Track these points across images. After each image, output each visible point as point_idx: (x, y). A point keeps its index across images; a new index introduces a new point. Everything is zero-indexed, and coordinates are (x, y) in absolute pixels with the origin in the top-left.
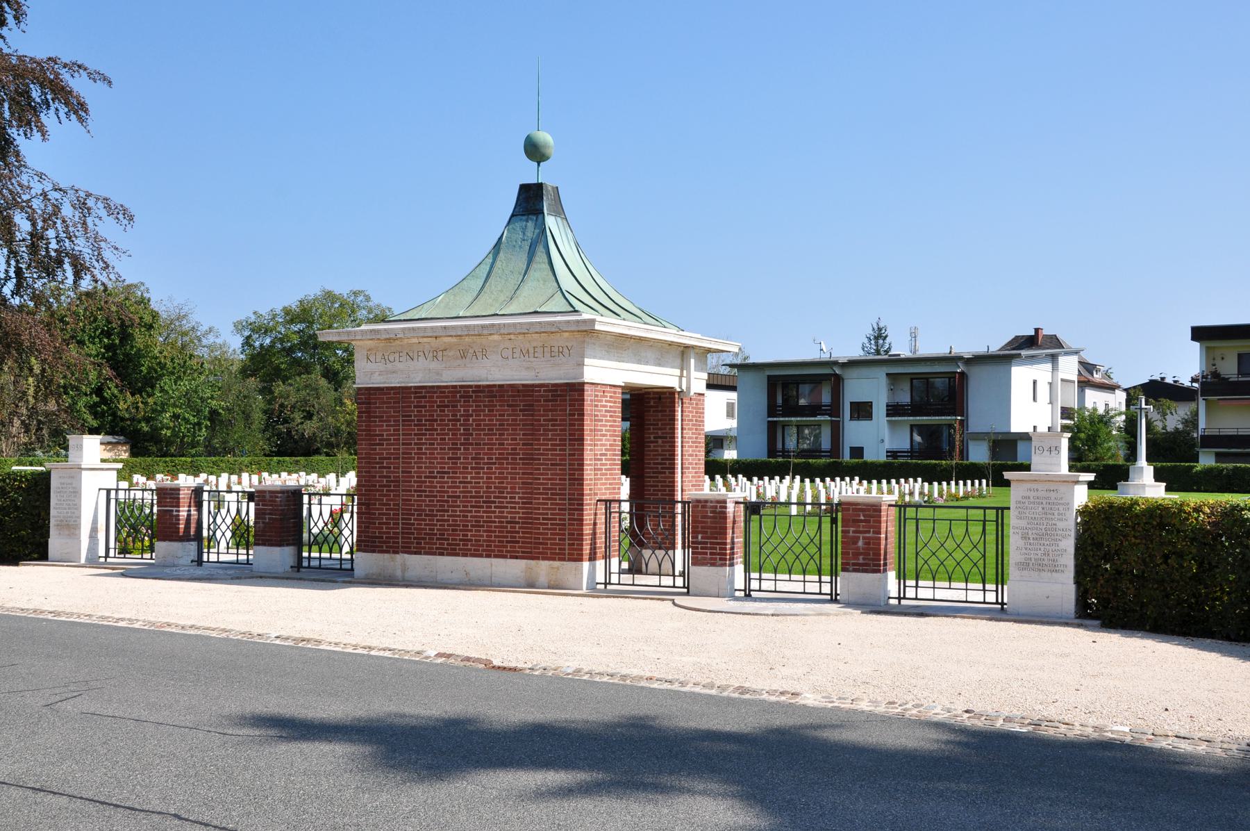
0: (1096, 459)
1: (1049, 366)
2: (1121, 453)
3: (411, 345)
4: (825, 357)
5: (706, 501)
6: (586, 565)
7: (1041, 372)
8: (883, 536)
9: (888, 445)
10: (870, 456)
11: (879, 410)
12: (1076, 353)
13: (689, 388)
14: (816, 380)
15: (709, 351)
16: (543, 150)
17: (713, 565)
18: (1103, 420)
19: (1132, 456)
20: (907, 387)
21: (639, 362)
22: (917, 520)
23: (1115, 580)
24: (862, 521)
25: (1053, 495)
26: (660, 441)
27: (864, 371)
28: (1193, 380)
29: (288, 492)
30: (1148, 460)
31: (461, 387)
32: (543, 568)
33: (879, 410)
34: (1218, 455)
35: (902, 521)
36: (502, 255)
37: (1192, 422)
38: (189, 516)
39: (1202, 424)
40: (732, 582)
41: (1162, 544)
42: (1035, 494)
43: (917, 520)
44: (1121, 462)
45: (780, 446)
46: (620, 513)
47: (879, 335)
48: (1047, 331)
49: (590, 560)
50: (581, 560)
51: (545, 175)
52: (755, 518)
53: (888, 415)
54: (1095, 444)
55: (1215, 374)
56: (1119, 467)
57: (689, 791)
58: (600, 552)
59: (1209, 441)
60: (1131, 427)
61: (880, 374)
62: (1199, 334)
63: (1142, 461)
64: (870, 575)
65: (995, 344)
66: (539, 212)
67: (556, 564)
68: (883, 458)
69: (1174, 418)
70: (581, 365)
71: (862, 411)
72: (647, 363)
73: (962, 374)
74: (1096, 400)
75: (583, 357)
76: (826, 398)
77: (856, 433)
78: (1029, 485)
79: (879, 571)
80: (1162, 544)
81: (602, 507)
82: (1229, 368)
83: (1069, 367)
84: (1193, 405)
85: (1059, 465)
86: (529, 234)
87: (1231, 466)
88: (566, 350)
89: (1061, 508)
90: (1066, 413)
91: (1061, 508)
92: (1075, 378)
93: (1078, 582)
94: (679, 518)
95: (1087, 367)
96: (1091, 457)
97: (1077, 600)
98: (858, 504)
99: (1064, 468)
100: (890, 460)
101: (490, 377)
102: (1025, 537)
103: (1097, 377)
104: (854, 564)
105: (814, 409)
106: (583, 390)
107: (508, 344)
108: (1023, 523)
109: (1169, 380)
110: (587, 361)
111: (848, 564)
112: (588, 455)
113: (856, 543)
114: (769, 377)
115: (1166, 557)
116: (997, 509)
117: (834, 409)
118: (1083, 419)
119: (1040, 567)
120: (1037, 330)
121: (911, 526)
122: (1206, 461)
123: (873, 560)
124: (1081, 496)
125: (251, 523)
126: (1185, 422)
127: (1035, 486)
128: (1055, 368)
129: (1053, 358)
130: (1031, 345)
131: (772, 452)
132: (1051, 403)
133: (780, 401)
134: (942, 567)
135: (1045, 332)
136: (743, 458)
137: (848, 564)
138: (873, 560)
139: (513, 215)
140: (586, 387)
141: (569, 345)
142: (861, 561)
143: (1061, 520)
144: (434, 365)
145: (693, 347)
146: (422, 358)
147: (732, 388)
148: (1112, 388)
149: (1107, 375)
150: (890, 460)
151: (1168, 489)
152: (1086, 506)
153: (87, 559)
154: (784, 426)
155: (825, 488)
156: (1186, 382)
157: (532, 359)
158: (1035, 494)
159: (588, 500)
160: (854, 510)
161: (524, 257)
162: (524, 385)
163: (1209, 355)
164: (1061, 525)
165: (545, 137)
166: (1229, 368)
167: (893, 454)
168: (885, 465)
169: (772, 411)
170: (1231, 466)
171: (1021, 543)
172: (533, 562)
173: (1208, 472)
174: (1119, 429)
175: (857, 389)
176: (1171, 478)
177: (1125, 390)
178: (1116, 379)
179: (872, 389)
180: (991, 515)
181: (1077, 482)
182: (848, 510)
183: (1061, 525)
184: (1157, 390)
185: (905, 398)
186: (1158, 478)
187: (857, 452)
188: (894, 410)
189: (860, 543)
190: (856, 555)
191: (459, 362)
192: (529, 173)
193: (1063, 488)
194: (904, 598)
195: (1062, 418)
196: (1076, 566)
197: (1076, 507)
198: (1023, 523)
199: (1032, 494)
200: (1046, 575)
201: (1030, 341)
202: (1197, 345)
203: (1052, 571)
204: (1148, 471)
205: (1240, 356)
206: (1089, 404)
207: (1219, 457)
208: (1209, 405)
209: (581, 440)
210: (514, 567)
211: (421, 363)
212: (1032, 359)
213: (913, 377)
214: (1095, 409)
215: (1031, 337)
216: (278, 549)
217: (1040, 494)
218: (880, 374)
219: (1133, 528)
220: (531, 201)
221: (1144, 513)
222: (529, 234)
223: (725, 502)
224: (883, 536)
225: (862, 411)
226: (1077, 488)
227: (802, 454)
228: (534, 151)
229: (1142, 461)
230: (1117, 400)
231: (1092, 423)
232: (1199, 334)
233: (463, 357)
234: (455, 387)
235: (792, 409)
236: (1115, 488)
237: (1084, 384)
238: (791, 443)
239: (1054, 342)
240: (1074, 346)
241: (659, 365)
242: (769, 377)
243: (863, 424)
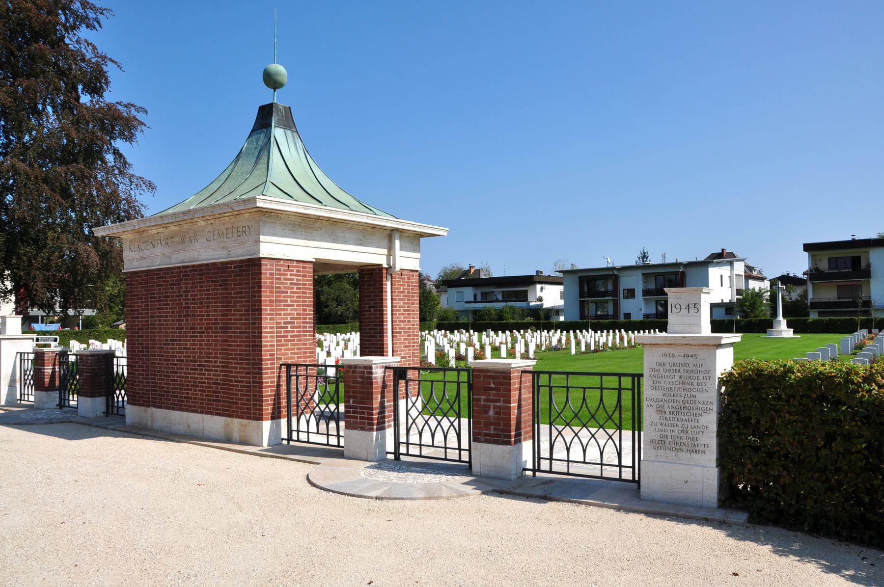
0: (755, 316)
1: (729, 267)
2: (768, 313)
3: (153, 235)
4: (610, 266)
5: (356, 367)
6: (267, 425)
7: (725, 271)
8: (514, 405)
9: (643, 312)
10: (634, 318)
11: (639, 293)
12: (743, 260)
13: (394, 264)
14: (605, 278)
15: (422, 235)
16: (275, 77)
17: (363, 429)
18: (759, 295)
19: (775, 314)
20: (653, 280)
21: (335, 241)
22: (551, 388)
23: (766, 464)
24: (492, 389)
25: (691, 361)
26: (372, 310)
27: (629, 272)
28: (804, 274)
29: (98, 355)
30: (784, 316)
31: (184, 267)
32: (236, 424)
33: (639, 293)
35: (536, 389)
36: (240, 162)
37: (805, 295)
38: (54, 372)
39: (810, 296)
40: (383, 445)
41: (824, 422)
42: (671, 360)
43: (551, 388)
44: (768, 318)
45: (586, 313)
46: (297, 376)
47: (644, 256)
48: (728, 250)
49: (273, 418)
50: (260, 418)
51: (276, 98)
52: (402, 383)
54: (754, 307)
55: (817, 269)
56: (768, 320)
58: (284, 411)
59: (815, 305)
60: (773, 298)
61: (639, 274)
62: (808, 247)
63: (780, 317)
64: (501, 446)
65: (702, 258)
66: (269, 125)
67: (245, 421)
68: (641, 318)
69: (796, 294)
70: (258, 242)
71: (631, 293)
72: (345, 242)
73: (682, 272)
74: (754, 285)
75: (259, 235)
76: (610, 287)
78: (664, 350)
79: (509, 443)
80: (824, 422)
81: (284, 369)
82: (824, 266)
83: (739, 268)
84: (804, 287)
85: (699, 325)
86: (260, 143)
87: (828, 318)
88: (247, 230)
89: (701, 376)
90: (739, 292)
91: (701, 376)
92: (743, 274)
93: (721, 463)
95: (749, 268)
96: (752, 315)
97: (721, 485)
98: (487, 371)
99: (706, 330)
100: (646, 320)
101: (200, 258)
102: (660, 411)
103: (755, 273)
104: (485, 435)
105: (605, 294)
106: (260, 265)
107: (210, 228)
108: (658, 394)
109: (791, 275)
110: (262, 238)
111: (480, 434)
112: (267, 323)
113: (487, 412)
114: (580, 277)
115: (830, 438)
116: (633, 376)
117: (615, 293)
118: (747, 294)
119: (677, 446)
120: (723, 250)
121: (544, 391)
122: (813, 316)
123: (503, 430)
124: (724, 362)
125: (125, 374)
126: (801, 296)
127: (671, 350)
129: (731, 263)
130: (721, 257)
131: (582, 316)
133: (586, 289)
134: (610, 413)
136: (569, 320)
137: (480, 434)
138: (503, 430)
139: (253, 131)
140: (263, 262)
141: (250, 224)
142: (492, 432)
143: (701, 391)
144: (167, 250)
145: (397, 230)
146: (159, 246)
147: (561, 284)
148: (762, 279)
149: (760, 272)
150: (646, 320)
151: (794, 332)
152: (731, 374)
153: (7, 401)
154: (588, 302)
155: (584, 337)
156: (800, 275)
157: (225, 240)
158: (671, 360)
159: (266, 364)
160: (485, 377)
161: (254, 160)
162: (221, 263)
163: (813, 259)
164: (701, 397)
165: (279, 69)
166: (824, 266)
167: (646, 316)
168: (641, 322)
169: (582, 294)
170: (828, 318)
171: (656, 417)
172: (229, 419)
173: (815, 322)
174: (767, 300)
175: (626, 282)
176: (797, 326)
177: (770, 280)
178: (764, 274)
179: (636, 282)
180: (627, 382)
181: (720, 346)
182: (479, 377)
183: (701, 397)
184: (786, 279)
185: (652, 286)
186: (789, 326)
187: (627, 316)
188: (646, 293)
189: (491, 413)
190: (488, 425)
191: (181, 246)
192: (267, 96)
193: (702, 353)
194: (539, 470)
196: (719, 445)
197: (718, 374)
198: (658, 394)
199: (667, 360)
200: (684, 455)
201: (720, 255)
202: (806, 254)
203: (692, 452)
204: (784, 322)
205: (829, 259)
206: (751, 287)
207: (820, 314)
208: (814, 287)
209: (259, 310)
210: (215, 423)
211: (159, 250)
212: (720, 264)
213: (656, 275)
214: (754, 289)
216: (89, 399)
217: (676, 360)
218: (639, 274)
219: (788, 401)
220: (265, 117)
221: (799, 382)
222: (260, 143)
223: (371, 368)
224: (514, 405)
225: (631, 293)
226: (719, 352)
227: (597, 317)
228: (271, 81)
229: (780, 317)
230: (766, 285)
231: (752, 296)
232: (808, 247)
233: (183, 242)
234: (179, 268)
235: (593, 293)
236: (765, 332)
237: (748, 277)
238: (592, 312)
239: (732, 255)
240: (740, 256)
241: (361, 245)
242: (580, 277)
243: (631, 301)
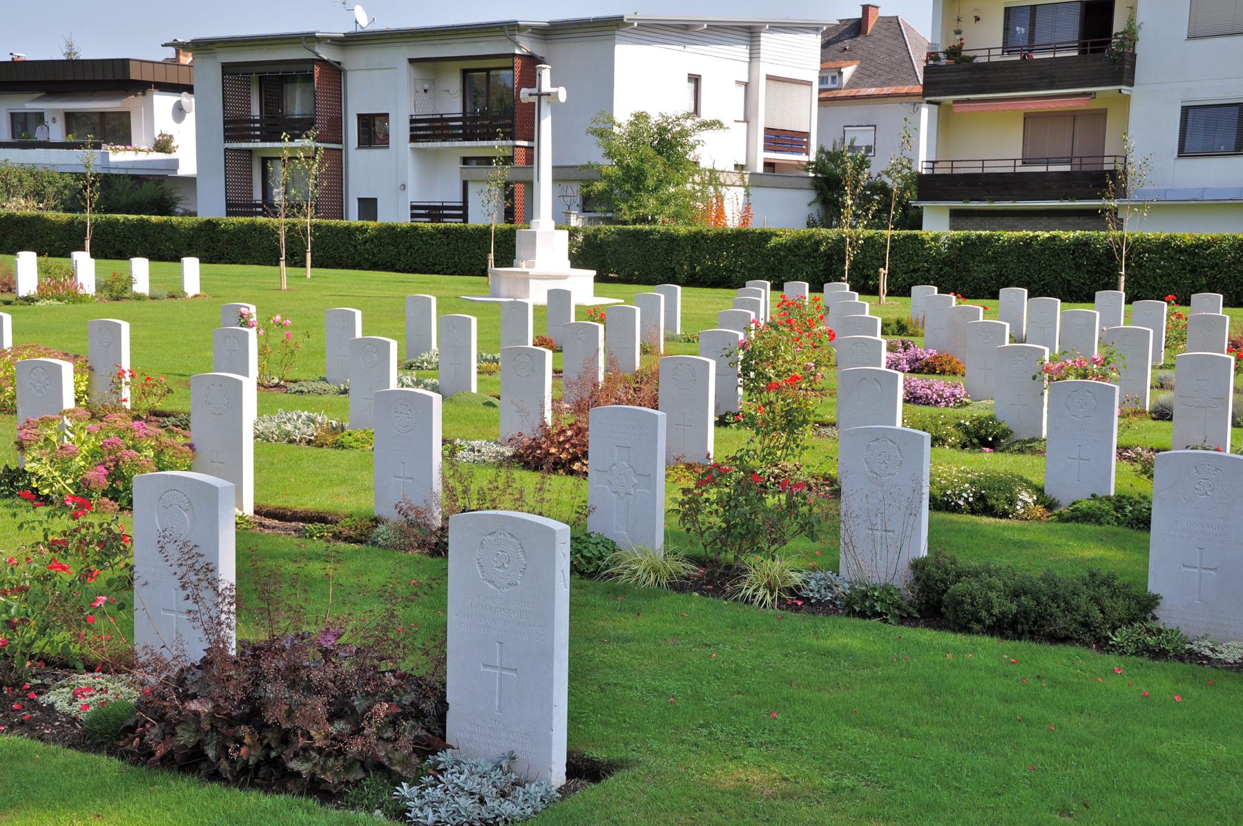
9: (416, 194)
20: (454, 84)
33: (399, 130)
34: (956, 215)
53: (413, 138)
57: (1077, 641)
71: (373, 131)
77: (367, 172)
94: (601, 345)
100: (426, 225)
117: (334, 132)
120: (866, 9)
128: (754, 56)
132: (746, 120)
135: (883, 12)
185: (452, 105)
195: (767, 148)
207: (957, 216)
215: (859, 20)
225: (373, 131)
243: (374, 155)
